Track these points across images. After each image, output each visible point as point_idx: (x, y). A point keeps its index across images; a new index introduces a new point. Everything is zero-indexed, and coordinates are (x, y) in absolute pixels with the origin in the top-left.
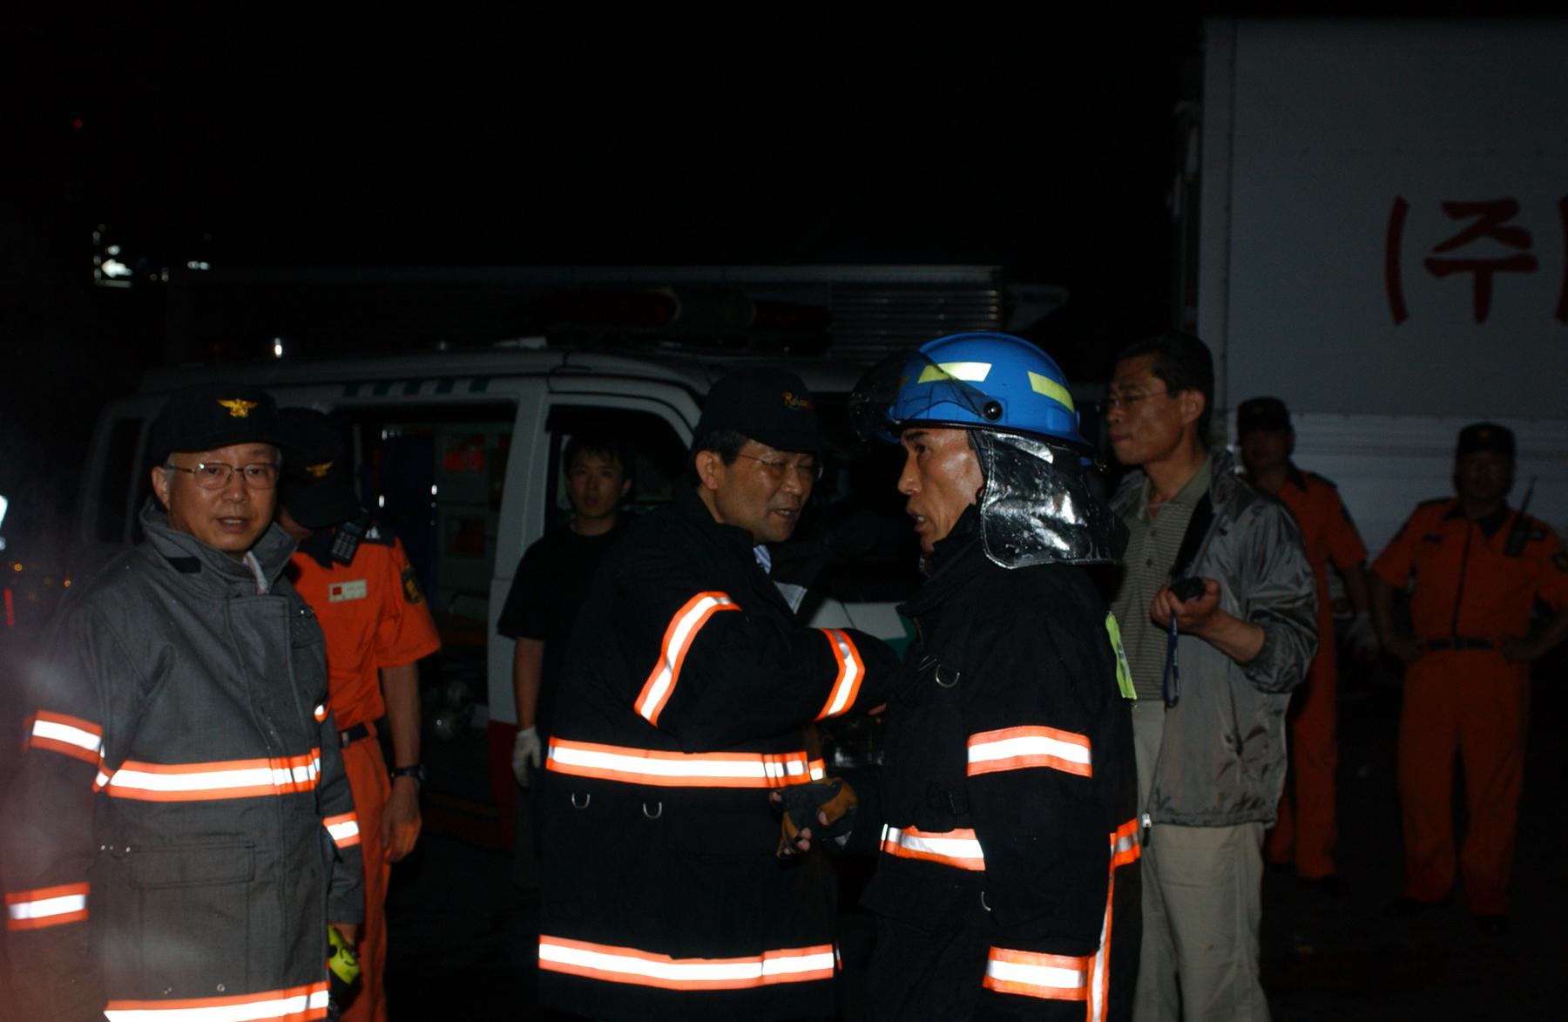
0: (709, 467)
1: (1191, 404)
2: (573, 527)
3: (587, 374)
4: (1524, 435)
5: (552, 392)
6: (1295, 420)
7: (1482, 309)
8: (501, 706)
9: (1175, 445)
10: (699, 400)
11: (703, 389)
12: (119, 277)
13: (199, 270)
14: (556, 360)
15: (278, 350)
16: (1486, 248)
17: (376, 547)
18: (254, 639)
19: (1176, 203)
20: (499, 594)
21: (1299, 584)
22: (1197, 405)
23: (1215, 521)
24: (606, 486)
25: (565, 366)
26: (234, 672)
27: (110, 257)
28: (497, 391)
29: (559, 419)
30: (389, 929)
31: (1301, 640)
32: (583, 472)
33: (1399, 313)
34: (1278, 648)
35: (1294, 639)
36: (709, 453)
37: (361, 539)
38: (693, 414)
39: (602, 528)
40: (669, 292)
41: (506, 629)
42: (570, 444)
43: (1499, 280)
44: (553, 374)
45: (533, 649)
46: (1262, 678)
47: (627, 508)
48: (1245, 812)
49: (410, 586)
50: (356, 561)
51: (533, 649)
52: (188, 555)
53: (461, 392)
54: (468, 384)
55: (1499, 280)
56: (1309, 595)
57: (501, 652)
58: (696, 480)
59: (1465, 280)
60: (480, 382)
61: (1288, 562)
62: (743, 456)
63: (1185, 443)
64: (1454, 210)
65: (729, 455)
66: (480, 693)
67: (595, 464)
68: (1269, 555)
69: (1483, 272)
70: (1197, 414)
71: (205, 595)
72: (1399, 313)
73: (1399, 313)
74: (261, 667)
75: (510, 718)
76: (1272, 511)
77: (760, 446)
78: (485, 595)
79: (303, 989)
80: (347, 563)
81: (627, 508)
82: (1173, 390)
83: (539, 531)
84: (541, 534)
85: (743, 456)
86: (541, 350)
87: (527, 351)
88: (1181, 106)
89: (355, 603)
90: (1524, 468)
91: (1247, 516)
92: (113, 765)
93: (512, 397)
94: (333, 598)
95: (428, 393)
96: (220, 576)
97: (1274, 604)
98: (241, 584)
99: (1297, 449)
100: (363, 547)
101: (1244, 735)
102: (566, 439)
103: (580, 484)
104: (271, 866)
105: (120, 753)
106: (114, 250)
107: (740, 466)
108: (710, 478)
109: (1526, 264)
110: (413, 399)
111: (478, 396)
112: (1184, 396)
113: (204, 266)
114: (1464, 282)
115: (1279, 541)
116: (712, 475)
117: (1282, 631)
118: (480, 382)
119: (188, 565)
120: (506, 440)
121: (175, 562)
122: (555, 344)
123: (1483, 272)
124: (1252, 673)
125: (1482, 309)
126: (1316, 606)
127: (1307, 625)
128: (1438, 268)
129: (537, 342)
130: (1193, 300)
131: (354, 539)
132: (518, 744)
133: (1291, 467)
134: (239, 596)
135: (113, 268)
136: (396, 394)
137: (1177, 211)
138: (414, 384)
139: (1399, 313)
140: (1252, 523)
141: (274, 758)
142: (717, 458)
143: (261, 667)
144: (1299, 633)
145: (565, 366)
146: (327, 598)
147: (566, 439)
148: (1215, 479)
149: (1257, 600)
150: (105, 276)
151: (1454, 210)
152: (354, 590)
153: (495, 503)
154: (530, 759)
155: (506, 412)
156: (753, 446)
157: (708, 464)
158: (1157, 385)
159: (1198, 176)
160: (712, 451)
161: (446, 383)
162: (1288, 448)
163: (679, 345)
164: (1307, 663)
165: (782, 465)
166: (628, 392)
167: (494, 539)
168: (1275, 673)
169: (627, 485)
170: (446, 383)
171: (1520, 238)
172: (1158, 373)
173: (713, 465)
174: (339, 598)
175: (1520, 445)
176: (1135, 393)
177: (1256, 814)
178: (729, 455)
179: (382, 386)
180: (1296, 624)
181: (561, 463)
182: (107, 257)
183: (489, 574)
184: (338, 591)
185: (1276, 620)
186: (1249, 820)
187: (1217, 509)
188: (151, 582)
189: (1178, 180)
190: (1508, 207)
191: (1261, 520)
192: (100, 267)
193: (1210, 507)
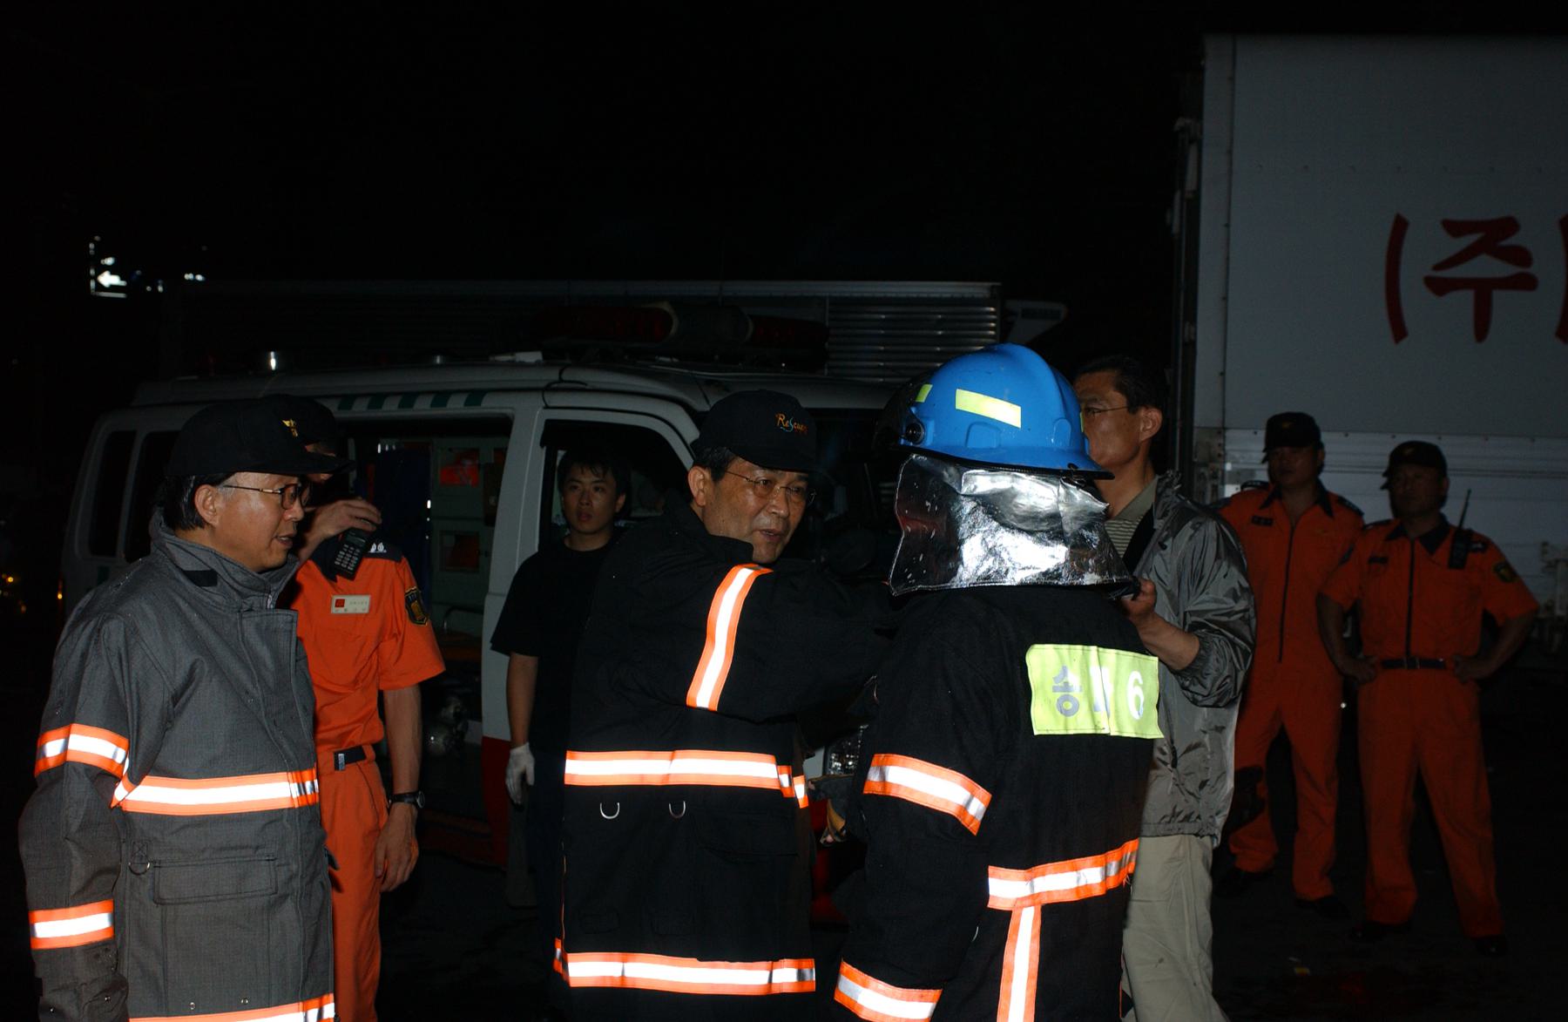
0: (701, 484)
1: (1150, 421)
2: (567, 544)
3: (583, 389)
4: (1453, 450)
5: (547, 407)
6: (1325, 437)
7: (1482, 327)
8: (495, 721)
9: (1129, 460)
10: (697, 418)
11: (702, 406)
12: (113, 288)
13: (195, 281)
14: (552, 375)
15: (273, 363)
16: (1486, 267)
17: (381, 562)
18: (264, 652)
19: (1175, 220)
20: (494, 608)
21: (1236, 599)
22: (1154, 422)
23: (1156, 536)
24: (599, 501)
25: (561, 380)
26: (250, 686)
27: (106, 268)
28: (492, 405)
29: (555, 434)
30: (383, 945)
31: (1235, 652)
32: (576, 487)
33: (1399, 331)
34: (1213, 658)
35: (1229, 651)
36: (700, 469)
37: (365, 553)
38: (691, 432)
39: (595, 544)
40: (666, 307)
41: (498, 645)
42: (565, 457)
43: (1499, 297)
44: (549, 388)
45: (527, 664)
46: (1197, 688)
47: (622, 523)
48: (1175, 825)
49: (415, 605)
50: (359, 576)
51: (527, 664)
52: (209, 569)
53: (456, 407)
54: (464, 397)
55: (1499, 297)
56: (1246, 610)
57: (494, 668)
58: (689, 497)
59: (1465, 299)
60: (475, 396)
61: (1225, 576)
62: (730, 473)
63: (1138, 462)
64: (1454, 228)
65: (718, 471)
66: (473, 710)
67: (587, 479)
68: (1207, 572)
69: (1483, 291)
70: (1155, 430)
71: (220, 609)
72: (1399, 331)
73: (1399, 330)
74: (271, 681)
75: (505, 735)
76: (1211, 528)
77: (747, 463)
78: (479, 610)
79: (775, 990)
80: (351, 576)
81: (622, 523)
82: (1133, 407)
83: (534, 547)
84: (537, 550)
85: (730, 473)
86: (536, 365)
87: (523, 365)
88: (1180, 123)
89: (356, 617)
90: (1456, 486)
91: (1187, 530)
92: (135, 779)
93: (508, 411)
94: (334, 610)
95: (423, 408)
96: (235, 590)
97: (1210, 616)
98: (252, 598)
99: (1326, 468)
100: (367, 562)
101: (1180, 749)
102: (561, 453)
103: (573, 499)
104: (291, 879)
105: (145, 766)
106: (109, 261)
107: (728, 482)
108: (701, 494)
109: (1526, 283)
110: (407, 413)
111: (474, 411)
112: (1142, 413)
113: (189, 276)
114: (1463, 301)
115: (1218, 557)
116: (703, 491)
117: (1217, 642)
118: (475, 396)
119: (206, 578)
120: (501, 454)
121: (191, 576)
122: (550, 359)
123: (1483, 291)
124: (1187, 683)
125: (1482, 327)
126: (1254, 622)
127: (1243, 638)
128: (1439, 286)
129: (533, 357)
130: (1192, 317)
131: (358, 551)
132: (511, 761)
133: (1319, 485)
134: (250, 610)
135: (107, 279)
136: (391, 409)
137: (1175, 229)
138: (409, 398)
139: (1399, 330)
140: (1191, 537)
141: (291, 771)
142: (707, 475)
143: (271, 684)
144: (1234, 645)
145: (561, 380)
146: (330, 610)
147: (561, 453)
148: (1159, 496)
149: (1192, 613)
150: (100, 287)
151: (1454, 228)
152: (357, 604)
153: (490, 519)
154: (523, 776)
155: (502, 426)
156: (740, 465)
157: (700, 480)
158: (1117, 399)
159: (1197, 193)
160: (704, 468)
161: (441, 397)
162: (1319, 468)
163: (675, 360)
164: (1241, 675)
165: (769, 483)
166: (630, 409)
167: (488, 554)
168: (1208, 683)
169: (621, 501)
170: (441, 397)
171: (1520, 256)
172: (1120, 388)
173: (704, 480)
174: (341, 610)
175: (1450, 463)
176: (1096, 406)
177: (1188, 827)
178: (718, 471)
179: (377, 399)
180: (1231, 636)
181: (555, 478)
182: (102, 269)
183: (483, 589)
184: (340, 603)
185: (1213, 631)
186: (1180, 832)
187: (1158, 524)
188: (173, 594)
189: (1178, 196)
190: (1509, 225)
191: (1199, 536)
192: (95, 278)
193: (1152, 523)
